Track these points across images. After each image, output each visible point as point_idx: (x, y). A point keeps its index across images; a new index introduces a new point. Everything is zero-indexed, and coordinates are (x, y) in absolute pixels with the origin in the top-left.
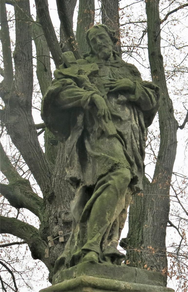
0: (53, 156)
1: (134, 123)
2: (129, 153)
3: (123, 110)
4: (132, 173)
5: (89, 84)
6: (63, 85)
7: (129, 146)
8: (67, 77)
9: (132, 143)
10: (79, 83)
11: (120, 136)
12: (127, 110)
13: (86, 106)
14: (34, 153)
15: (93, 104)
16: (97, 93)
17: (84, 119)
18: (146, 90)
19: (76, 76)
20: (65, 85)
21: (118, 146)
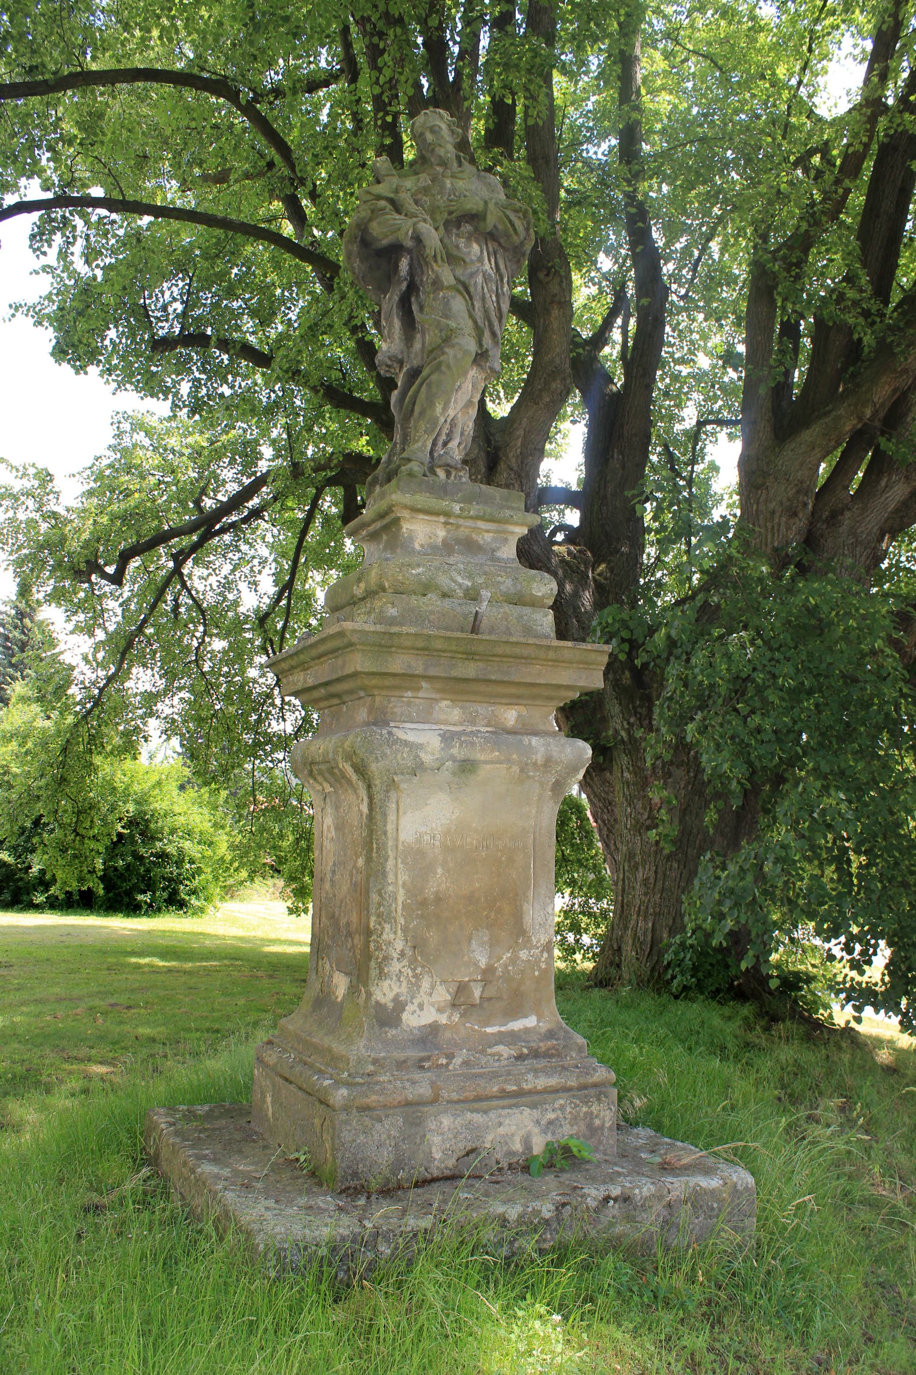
0: (362, 694)
1: (487, 267)
2: (479, 314)
3: (468, 245)
4: (480, 345)
5: (413, 208)
6: (373, 211)
7: (478, 305)
8: (379, 197)
9: (483, 299)
10: (397, 207)
11: (464, 288)
12: (475, 247)
13: (409, 243)
14: (255, 502)
15: (418, 239)
16: (425, 221)
17: (411, 265)
18: (507, 217)
19: (392, 195)
20: (375, 212)
21: (458, 304)
